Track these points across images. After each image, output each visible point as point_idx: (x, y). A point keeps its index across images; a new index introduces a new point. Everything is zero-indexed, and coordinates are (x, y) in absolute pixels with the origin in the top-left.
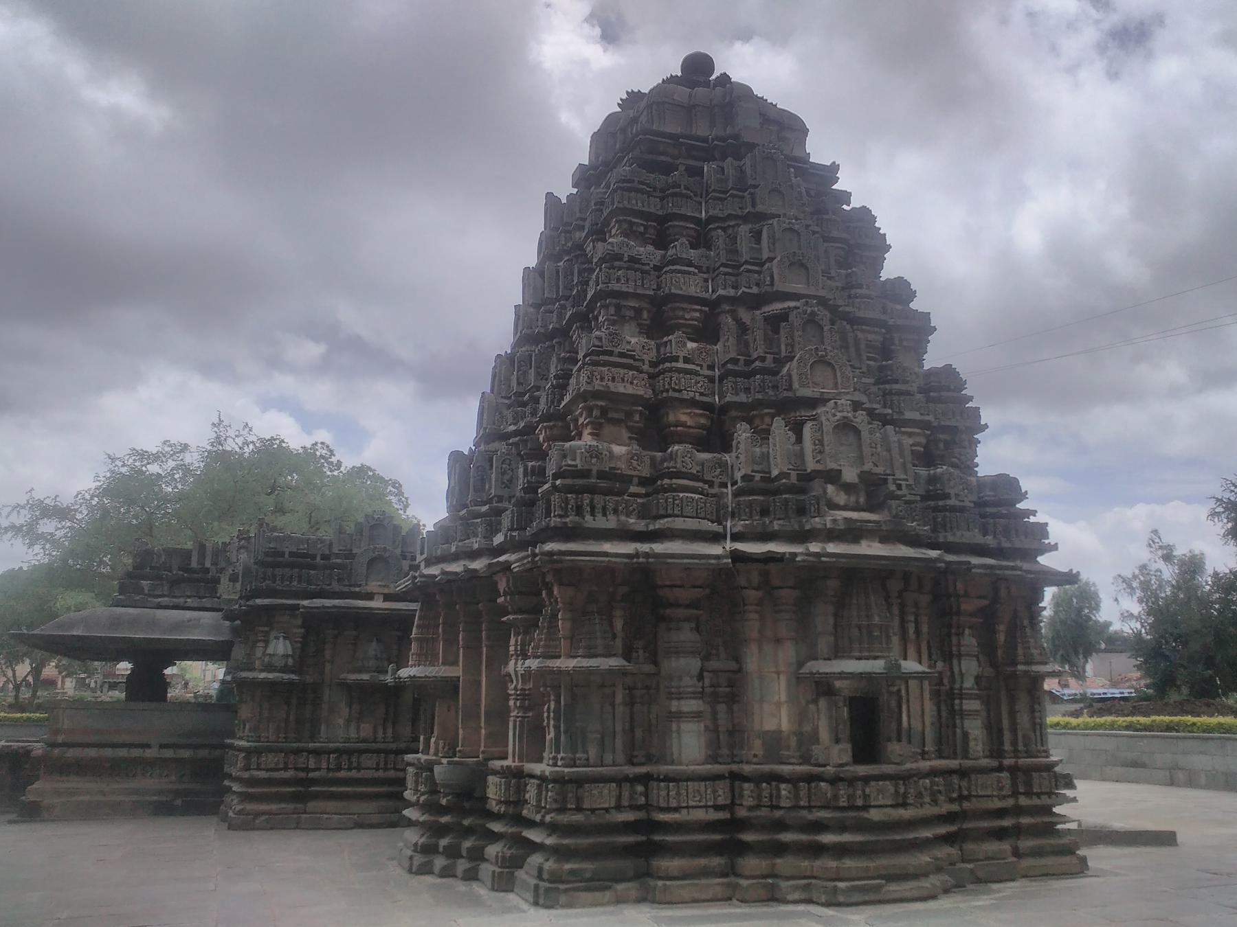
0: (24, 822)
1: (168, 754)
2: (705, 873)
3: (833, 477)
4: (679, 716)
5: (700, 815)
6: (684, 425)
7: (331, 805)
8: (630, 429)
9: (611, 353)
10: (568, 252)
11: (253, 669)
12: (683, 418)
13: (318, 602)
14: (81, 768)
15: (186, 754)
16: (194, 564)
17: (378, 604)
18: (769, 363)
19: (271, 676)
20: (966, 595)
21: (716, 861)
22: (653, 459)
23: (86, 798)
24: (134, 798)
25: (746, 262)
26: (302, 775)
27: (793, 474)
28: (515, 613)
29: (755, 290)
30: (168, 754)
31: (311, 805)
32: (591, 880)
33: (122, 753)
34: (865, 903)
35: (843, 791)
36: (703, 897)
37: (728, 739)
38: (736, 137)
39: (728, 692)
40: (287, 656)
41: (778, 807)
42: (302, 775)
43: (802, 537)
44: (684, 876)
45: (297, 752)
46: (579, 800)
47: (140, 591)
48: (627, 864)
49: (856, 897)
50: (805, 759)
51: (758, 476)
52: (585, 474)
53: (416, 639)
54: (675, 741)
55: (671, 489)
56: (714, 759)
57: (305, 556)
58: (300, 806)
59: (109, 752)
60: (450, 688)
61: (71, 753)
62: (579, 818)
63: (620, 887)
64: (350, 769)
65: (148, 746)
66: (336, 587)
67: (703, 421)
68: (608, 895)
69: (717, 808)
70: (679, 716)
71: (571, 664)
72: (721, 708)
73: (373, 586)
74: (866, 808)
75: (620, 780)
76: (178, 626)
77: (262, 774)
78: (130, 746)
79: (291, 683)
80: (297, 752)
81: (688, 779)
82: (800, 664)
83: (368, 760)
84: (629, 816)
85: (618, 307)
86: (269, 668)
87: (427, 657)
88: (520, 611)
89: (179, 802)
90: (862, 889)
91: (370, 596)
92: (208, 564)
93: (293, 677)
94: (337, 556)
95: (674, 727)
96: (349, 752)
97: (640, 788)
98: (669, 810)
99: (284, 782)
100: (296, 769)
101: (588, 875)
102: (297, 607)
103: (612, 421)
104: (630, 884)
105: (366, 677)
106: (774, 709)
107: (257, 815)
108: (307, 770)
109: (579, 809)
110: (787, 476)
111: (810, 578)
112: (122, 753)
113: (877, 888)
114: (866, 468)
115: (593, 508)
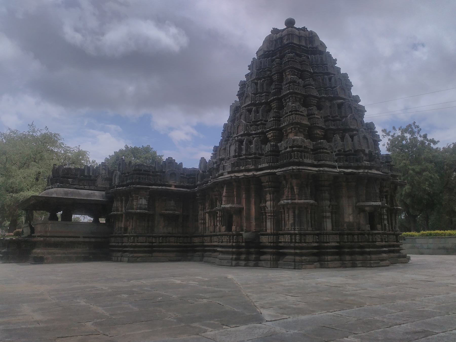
0: (35, 264)
1: (87, 240)
2: (335, 260)
3: (363, 151)
4: (326, 217)
5: (334, 244)
6: (318, 134)
7: (161, 254)
8: (304, 134)
9: (299, 111)
10: (264, 78)
11: (133, 209)
12: (318, 132)
13: (154, 187)
14: (56, 245)
15: (93, 240)
16: (86, 174)
17: (173, 188)
18: (338, 118)
19: (142, 211)
20: (385, 187)
21: (337, 257)
22: (313, 144)
23: (60, 255)
24: (76, 255)
25: (328, 87)
26: (151, 244)
27: (353, 150)
28: (269, 188)
29: (332, 96)
30: (87, 240)
31: (154, 254)
32: (309, 262)
33: (71, 239)
34: (376, 267)
35: (371, 237)
36: (336, 266)
37: (336, 224)
38: (313, 48)
39: (337, 211)
40: (145, 205)
41: (353, 242)
42: (151, 244)
43: (358, 168)
44: (331, 261)
45: (149, 237)
46: (305, 239)
47: (68, 182)
48: (316, 258)
49: (375, 265)
50: (359, 230)
51: (343, 150)
52: (300, 147)
53: (225, 196)
54: (325, 224)
55: (323, 153)
56: (332, 230)
57: (147, 171)
58: (150, 255)
59: (67, 239)
60: (239, 211)
61: (53, 239)
62: (305, 244)
63: (315, 264)
64: (166, 242)
65: (79, 237)
66: (159, 182)
67: (323, 133)
68: (313, 266)
69: (337, 242)
70: (326, 217)
71: (302, 201)
72: (334, 215)
73: (171, 182)
74: (375, 242)
75: (314, 234)
76: (88, 195)
77: (139, 244)
78: (74, 237)
79: (145, 214)
80: (149, 237)
81: (330, 234)
82: (356, 203)
83: (172, 239)
84: (316, 244)
85: (296, 97)
86: (140, 209)
87: (228, 202)
88: (271, 187)
89: (91, 257)
90: (376, 263)
91: (170, 186)
92: (91, 174)
93: (147, 211)
94: (158, 172)
95: (325, 220)
96: (166, 237)
97: (317, 237)
98: (327, 243)
99: (146, 247)
100: (149, 242)
101: (308, 260)
102: (149, 189)
103: (301, 132)
104: (318, 263)
105: (171, 212)
106: (349, 216)
107: (138, 257)
108: (152, 243)
109: (305, 242)
110: (351, 150)
111: (358, 178)
112: (71, 239)
113: (379, 263)
114: (370, 150)
115: (305, 156)
